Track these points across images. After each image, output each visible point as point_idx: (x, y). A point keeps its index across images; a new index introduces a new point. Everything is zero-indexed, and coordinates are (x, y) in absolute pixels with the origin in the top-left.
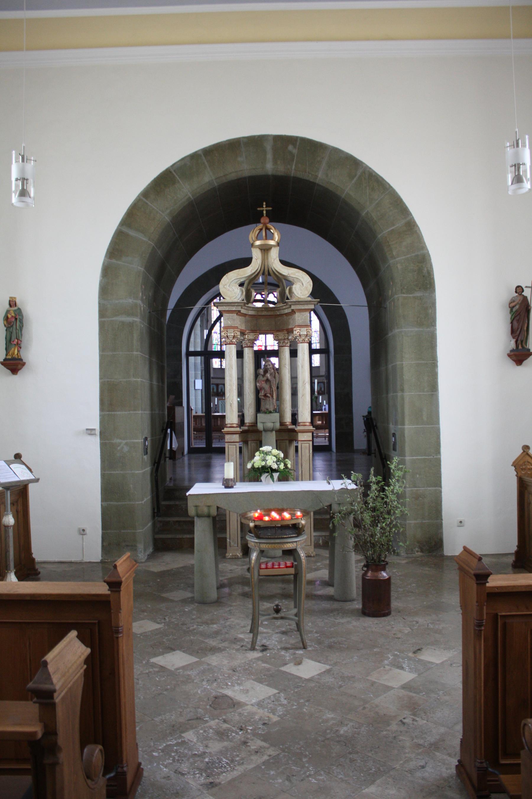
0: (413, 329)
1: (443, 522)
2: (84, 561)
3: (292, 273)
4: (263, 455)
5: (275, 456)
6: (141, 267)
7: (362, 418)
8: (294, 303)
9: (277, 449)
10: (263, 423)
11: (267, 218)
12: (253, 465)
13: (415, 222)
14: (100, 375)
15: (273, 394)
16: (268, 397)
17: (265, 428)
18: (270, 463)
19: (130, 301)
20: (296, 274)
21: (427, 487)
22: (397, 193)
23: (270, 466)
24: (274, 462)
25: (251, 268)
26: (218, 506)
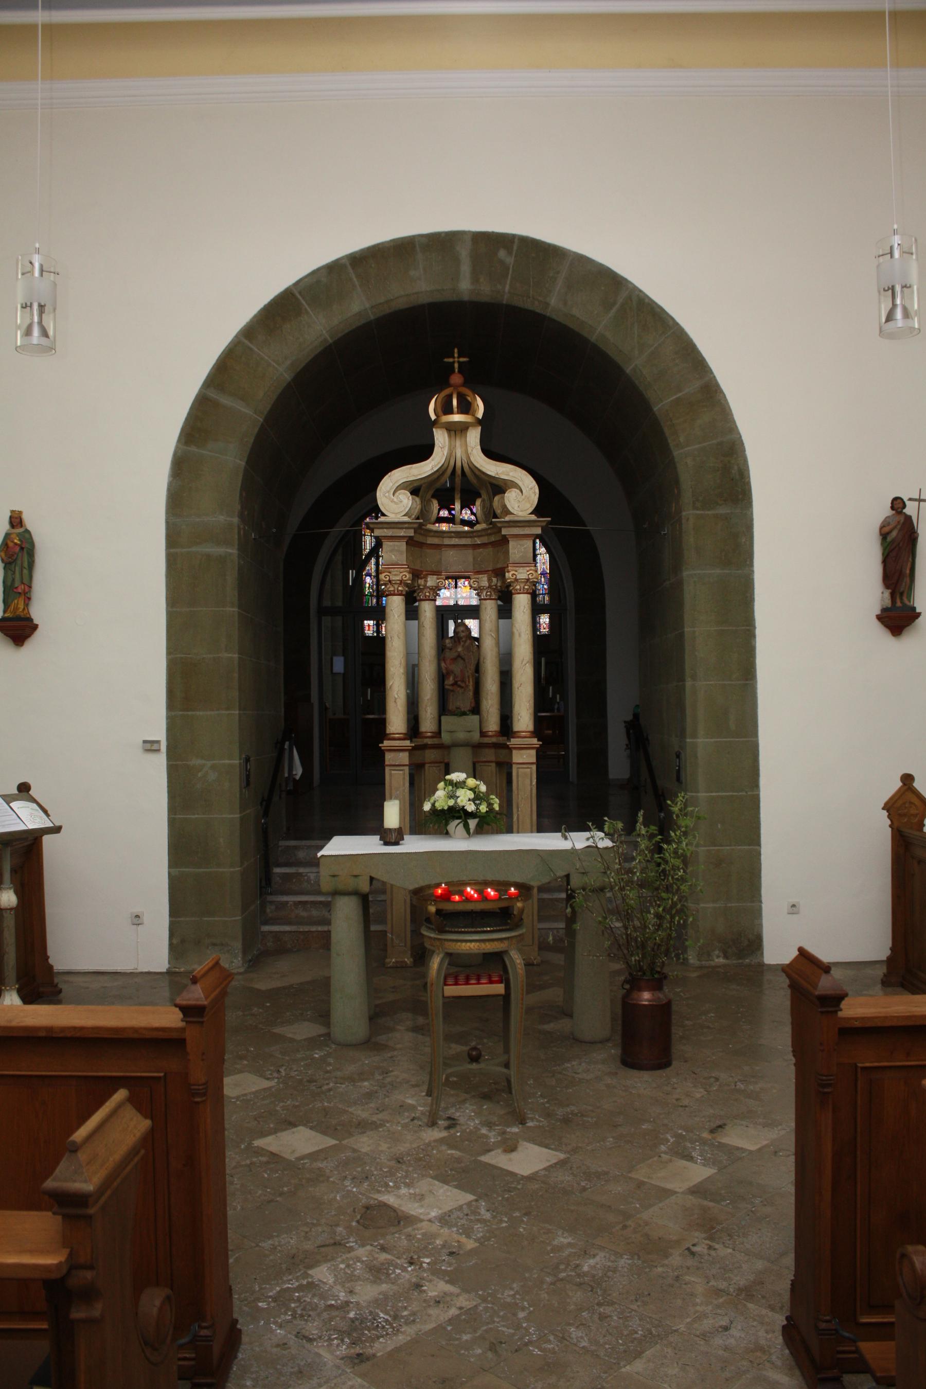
0: (713, 571)
1: (763, 906)
2: (138, 971)
3: (502, 473)
4: (450, 788)
5: (471, 789)
6: (241, 460)
7: (624, 724)
9: (475, 777)
11: (460, 375)
12: (433, 805)
13: (717, 385)
14: (168, 648)
18: (462, 801)
19: (222, 518)
21: (735, 846)
22: (686, 335)
23: (464, 807)
24: (469, 800)
26: (373, 875)
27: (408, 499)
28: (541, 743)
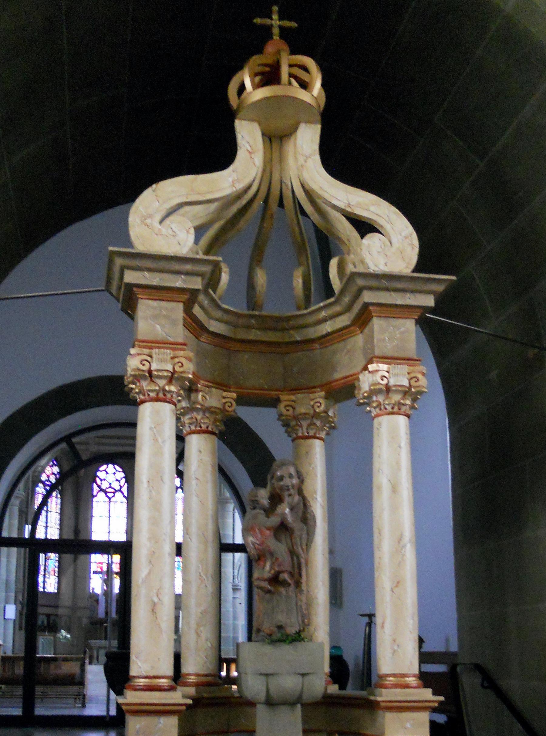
3: (359, 205)
8: (373, 283)
10: (267, 675)
15: (300, 575)
16: (284, 583)
17: (272, 691)
20: (372, 208)
25: (234, 176)
27: (188, 232)
28: (442, 698)
